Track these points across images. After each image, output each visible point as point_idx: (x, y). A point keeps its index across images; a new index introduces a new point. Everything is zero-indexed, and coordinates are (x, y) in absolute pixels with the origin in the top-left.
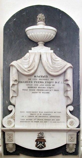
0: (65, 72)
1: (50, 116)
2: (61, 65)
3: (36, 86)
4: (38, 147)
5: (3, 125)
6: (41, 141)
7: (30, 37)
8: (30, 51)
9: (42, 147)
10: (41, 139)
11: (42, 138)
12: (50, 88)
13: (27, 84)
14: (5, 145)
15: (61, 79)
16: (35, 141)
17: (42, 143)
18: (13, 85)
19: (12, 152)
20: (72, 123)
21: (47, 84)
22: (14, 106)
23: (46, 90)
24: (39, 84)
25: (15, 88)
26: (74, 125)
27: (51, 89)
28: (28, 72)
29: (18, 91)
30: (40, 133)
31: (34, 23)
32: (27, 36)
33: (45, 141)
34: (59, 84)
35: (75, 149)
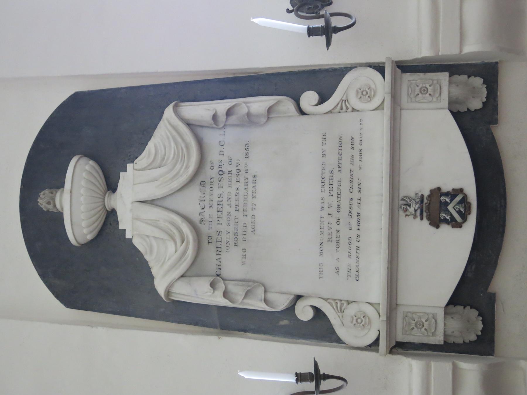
0: (189, 125)
1: (336, 172)
2: (168, 138)
3: (232, 218)
4: (464, 217)
5: (370, 346)
6: (437, 208)
7: (91, 232)
8: (128, 236)
9: (465, 201)
10: (428, 208)
11: (425, 201)
12: (239, 171)
13: (224, 249)
14: (448, 348)
15: (212, 137)
16: (438, 230)
17: (447, 204)
18: (225, 294)
19: (481, 322)
20: (364, 93)
21: (225, 183)
22: (298, 297)
23: (246, 187)
24: (226, 209)
25: (238, 291)
26: (373, 86)
27: (242, 167)
28: (188, 243)
29: (249, 281)
30: (405, 210)
31: (58, 217)
32: (92, 241)
33: (439, 189)
34: (224, 144)
35: (469, 77)
